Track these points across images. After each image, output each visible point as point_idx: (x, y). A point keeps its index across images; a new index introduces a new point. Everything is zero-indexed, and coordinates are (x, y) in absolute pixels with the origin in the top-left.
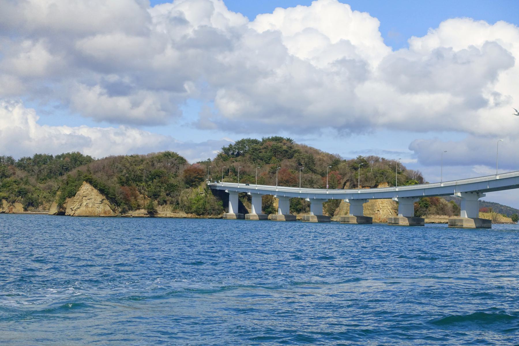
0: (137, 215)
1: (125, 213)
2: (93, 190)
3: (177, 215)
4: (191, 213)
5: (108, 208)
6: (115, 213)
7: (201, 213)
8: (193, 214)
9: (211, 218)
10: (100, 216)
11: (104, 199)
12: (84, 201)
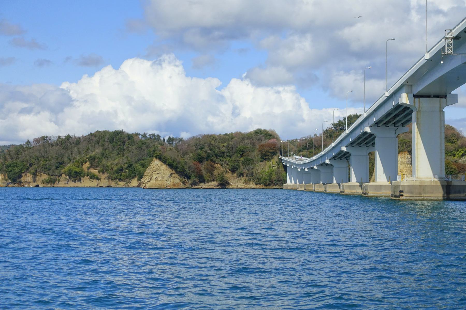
0: (207, 187)
1: (195, 185)
2: (162, 165)
3: (248, 186)
4: (260, 184)
5: (177, 181)
6: (186, 185)
7: (268, 184)
8: (262, 185)
9: (276, 188)
10: (167, 188)
11: (173, 173)
12: (154, 175)
